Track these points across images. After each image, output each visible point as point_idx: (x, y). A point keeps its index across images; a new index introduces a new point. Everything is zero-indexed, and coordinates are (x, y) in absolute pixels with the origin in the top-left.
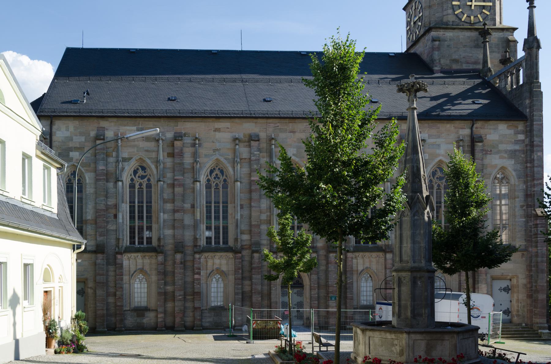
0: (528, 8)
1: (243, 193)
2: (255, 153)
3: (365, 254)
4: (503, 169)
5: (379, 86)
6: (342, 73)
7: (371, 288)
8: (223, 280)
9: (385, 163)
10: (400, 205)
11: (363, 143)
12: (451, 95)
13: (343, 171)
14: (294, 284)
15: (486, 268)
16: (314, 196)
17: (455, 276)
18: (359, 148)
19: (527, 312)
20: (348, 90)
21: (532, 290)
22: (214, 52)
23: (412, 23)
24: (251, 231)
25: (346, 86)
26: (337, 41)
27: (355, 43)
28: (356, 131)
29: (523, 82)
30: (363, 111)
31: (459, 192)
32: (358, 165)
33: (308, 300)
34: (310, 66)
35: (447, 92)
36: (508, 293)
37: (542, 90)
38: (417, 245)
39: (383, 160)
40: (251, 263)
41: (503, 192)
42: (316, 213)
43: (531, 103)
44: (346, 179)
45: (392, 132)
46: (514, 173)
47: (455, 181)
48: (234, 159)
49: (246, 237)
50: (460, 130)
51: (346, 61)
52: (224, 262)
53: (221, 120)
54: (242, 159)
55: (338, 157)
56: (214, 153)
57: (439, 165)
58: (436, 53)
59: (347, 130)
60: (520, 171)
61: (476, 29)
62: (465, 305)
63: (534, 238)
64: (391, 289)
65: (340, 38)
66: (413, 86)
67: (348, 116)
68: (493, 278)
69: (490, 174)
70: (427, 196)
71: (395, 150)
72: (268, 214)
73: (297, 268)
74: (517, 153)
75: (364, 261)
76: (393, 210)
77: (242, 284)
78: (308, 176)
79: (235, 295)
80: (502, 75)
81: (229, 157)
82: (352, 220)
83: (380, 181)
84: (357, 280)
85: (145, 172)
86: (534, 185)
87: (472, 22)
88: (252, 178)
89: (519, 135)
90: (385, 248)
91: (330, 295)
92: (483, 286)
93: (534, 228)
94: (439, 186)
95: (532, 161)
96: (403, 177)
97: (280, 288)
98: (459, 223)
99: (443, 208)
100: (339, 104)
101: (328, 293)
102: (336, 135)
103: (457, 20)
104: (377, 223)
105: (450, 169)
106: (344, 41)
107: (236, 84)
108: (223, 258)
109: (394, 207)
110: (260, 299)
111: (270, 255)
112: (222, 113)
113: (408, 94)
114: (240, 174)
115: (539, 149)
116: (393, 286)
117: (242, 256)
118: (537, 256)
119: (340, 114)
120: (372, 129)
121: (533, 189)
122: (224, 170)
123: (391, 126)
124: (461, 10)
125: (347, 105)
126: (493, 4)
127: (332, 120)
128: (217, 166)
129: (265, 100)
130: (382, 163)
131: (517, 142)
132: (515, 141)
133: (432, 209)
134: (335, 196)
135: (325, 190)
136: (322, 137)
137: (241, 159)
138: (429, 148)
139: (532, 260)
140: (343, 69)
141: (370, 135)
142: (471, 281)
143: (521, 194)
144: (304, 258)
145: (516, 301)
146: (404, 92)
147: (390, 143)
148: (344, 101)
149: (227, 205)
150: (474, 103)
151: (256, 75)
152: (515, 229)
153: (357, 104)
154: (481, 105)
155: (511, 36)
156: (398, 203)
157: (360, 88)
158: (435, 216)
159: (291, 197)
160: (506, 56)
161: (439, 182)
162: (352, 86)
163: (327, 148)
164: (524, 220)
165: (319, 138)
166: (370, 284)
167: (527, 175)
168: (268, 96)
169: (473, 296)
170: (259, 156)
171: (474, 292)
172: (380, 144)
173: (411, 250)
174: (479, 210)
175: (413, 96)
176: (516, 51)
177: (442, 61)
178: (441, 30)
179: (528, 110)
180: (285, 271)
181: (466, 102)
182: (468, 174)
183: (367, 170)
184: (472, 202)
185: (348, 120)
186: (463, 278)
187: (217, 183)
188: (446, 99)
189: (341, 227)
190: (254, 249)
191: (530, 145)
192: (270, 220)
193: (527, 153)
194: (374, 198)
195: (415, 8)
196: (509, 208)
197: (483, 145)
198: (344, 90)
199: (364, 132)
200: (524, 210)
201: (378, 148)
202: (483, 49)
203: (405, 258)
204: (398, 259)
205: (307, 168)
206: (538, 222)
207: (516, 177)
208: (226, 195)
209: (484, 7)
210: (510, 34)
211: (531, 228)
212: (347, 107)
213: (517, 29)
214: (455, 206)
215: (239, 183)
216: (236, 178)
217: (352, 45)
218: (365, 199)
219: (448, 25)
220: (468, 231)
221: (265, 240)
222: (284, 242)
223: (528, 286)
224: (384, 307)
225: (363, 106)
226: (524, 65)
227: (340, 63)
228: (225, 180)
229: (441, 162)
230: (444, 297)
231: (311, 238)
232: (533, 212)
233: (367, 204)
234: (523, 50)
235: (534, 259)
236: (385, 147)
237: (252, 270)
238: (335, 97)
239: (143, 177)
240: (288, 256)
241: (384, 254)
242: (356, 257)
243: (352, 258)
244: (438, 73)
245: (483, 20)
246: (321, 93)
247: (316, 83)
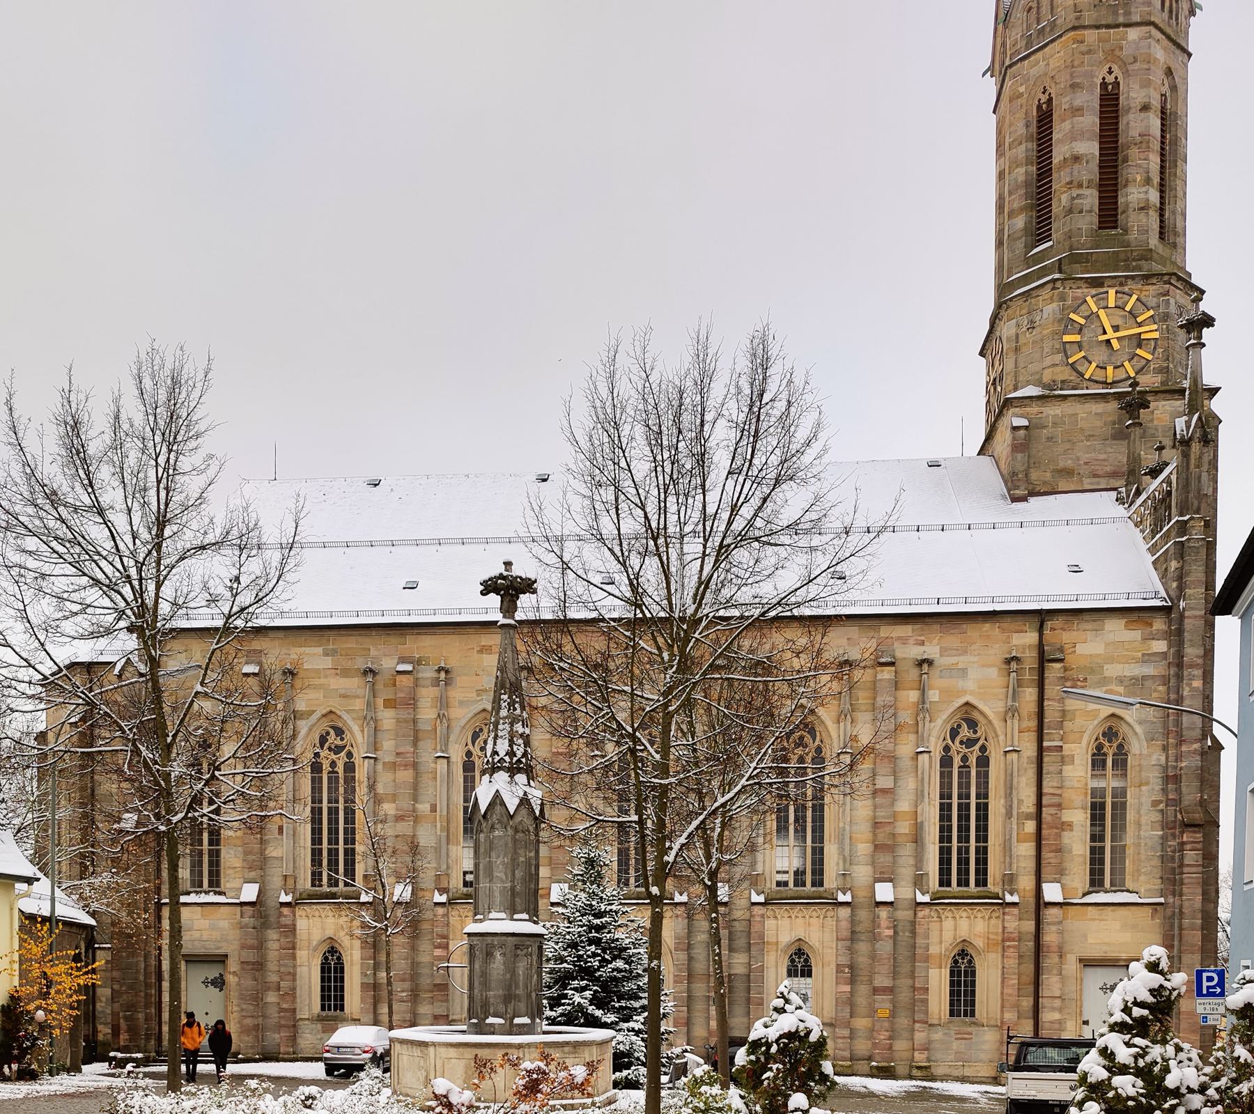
60: (1153, 723)
74: (1148, 683)
85: (342, 739)
87: (1109, 381)
89: (1154, 643)
124: (1082, 354)
131: (1147, 658)
132: (1143, 655)
164: (1161, 833)
197: (1064, 667)
206: (1185, 839)
207: (1143, 737)
239: (337, 750)
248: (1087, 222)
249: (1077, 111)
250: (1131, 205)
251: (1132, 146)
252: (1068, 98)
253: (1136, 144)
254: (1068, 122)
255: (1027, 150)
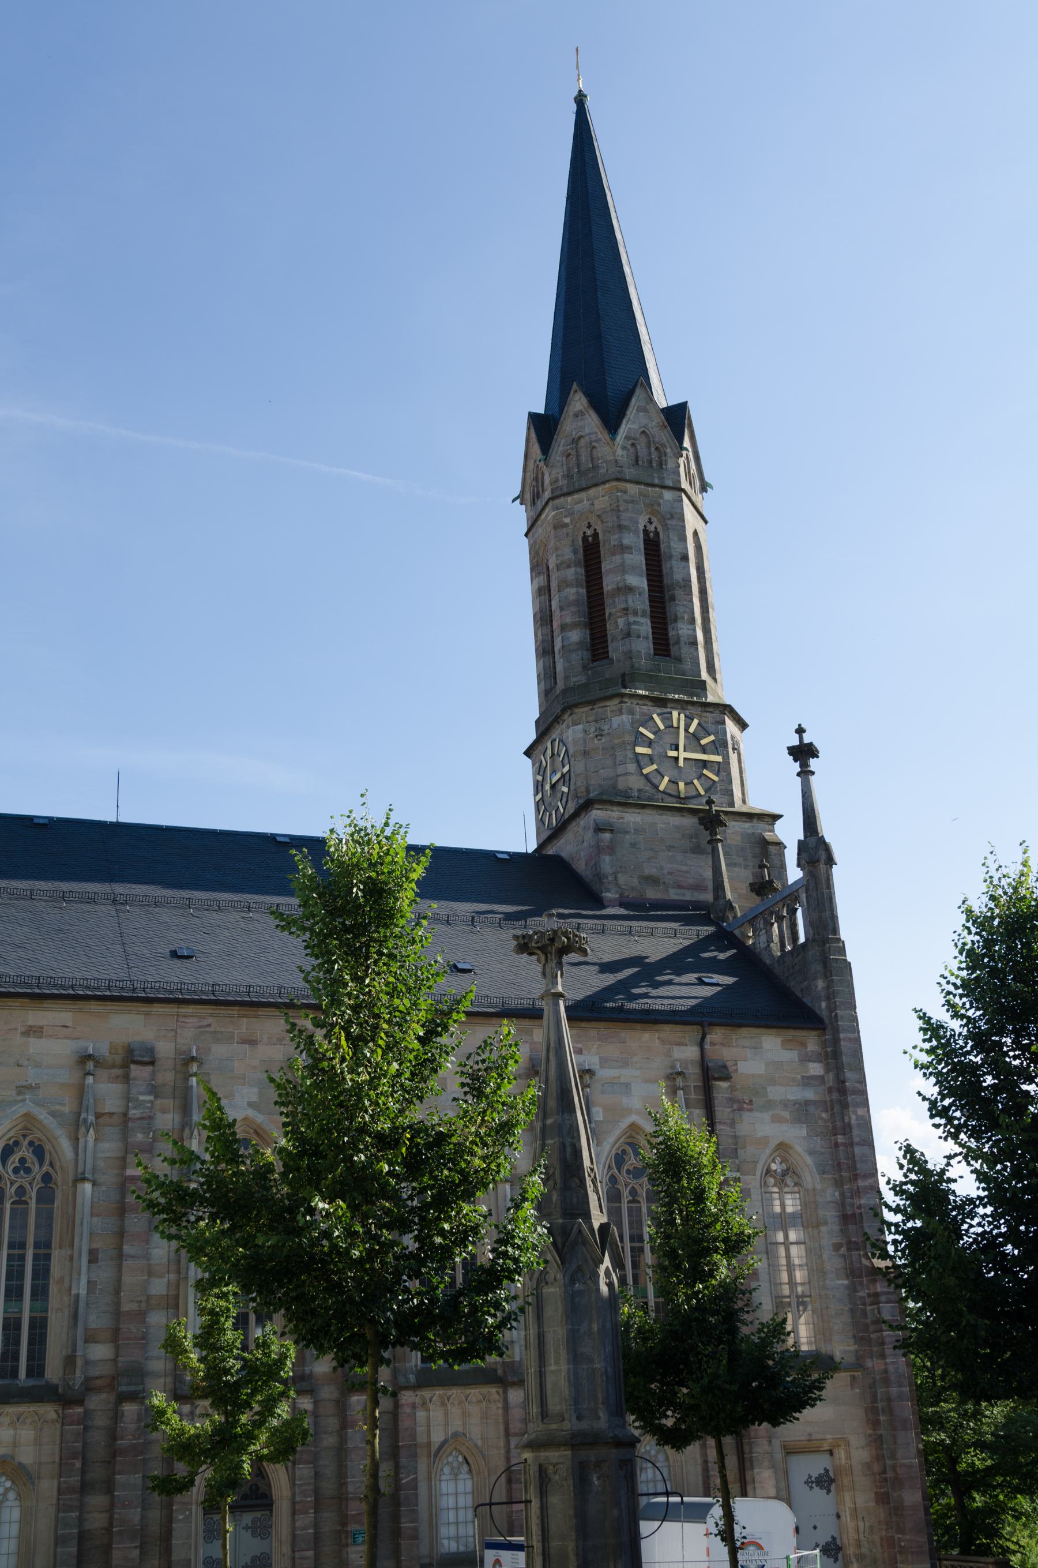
0: (798, 774)
1: (98, 1215)
2: (141, 1098)
3: (449, 1393)
4: (783, 1148)
5: (475, 930)
6: (374, 902)
7: (469, 1498)
8: (19, 1497)
9: (490, 1142)
10: (532, 1256)
11: (431, 1083)
12: (647, 961)
13: (378, 1162)
14: (245, 1497)
15: (765, 1424)
16: (300, 1231)
17: (693, 1450)
18: (421, 1098)
19: (882, 1546)
20: (390, 945)
21: (886, 1480)
22: (41, 821)
23: (547, 787)
24: (116, 1331)
25: (385, 936)
26: (361, 824)
27: (406, 832)
28: (412, 1051)
29: (807, 939)
30: (429, 1001)
31: (681, 1211)
32: (418, 1144)
33: (286, 1549)
34: (291, 881)
35: (638, 954)
36: (829, 1492)
37: (849, 958)
38: (585, 1367)
39: (482, 1131)
40: (113, 1435)
41: (789, 1209)
42: (304, 1282)
43: (828, 987)
44: (388, 1183)
45: (504, 1058)
46: (809, 1160)
47: (670, 1184)
48: (79, 1114)
49: (101, 1351)
50: (676, 1048)
51: (383, 873)
52: (27, 1434)
53: (48, 1004)
54: (104, 1114)
55: (365, 1123)
56: (20, 1098)
57: (630, 1137)
58: (607, 859)
59: (389, 1048)
60: (822, 1154)
61: (693, 812)
62: (723, 1539)
63: (876, 1332)
64: (521, 1502)
65: (369, 817)
66: (552, 940)
67: (390, 1013)
68: (790, 1451)
69: (755, 1162)
70: (602, 1226)
71: (512, 1107)
72: (173, 1276)
73: (252, 1448)
75: (446, 1414)
76: (515, 1270)
77: (82, 1508)
78: (284, 1175)
79: (56, 1545)
80: (760, 919)
81: (62, 1108)
82: (406, 1301)
83: (476, 1188)
84: (430, 1473)
86: (859, 1192)
88: (130, 1172)
90: (504, 1372)
91: (352, 1527)
92: (764, 1476)
93: (872, 1304)
94: (633, 1192)
95: (847, 1129)
96: (536, 1178)
97: (201, 1512)
98: (688, 1299)
99: (648, 1258)
100: (367, 981)
101: (344, 1521)
102: (357, 1061)
103: (648, 788)
104: (474, 1308)
105: (655, 1151)
106: (379, 825)
107: (97, 908)
108: (24, 1422)
109: (516, 1261)
110: (136, 1552)
111: (170, 1411)
112: (49, 986)
113: (543, 957)
114: (94, 1157)
115: (859, 1099)
116: (526, 1492)
117: (87, 1413)
118: (886, 1381)
119: (371, 1006)
120: (453, 1048)
121: (857, 1202)
122: (48, 1147)
123: (501, 1041)
124: (655, 767)
125: (387, 984)
126: (723, 758)
127: (349, 1022)
128: (25, 1136)
129: (174, 955)
130: (481, 1138)
131: (808, 1081)
132: (803, 1077)
133: (618, 1263)
134: (356, 1233)
135: (328, 1214)
136: (320, 1066)
137: (98, 1116)
138: (603, 1092)
139: (876, 1393)
140: (377, 891)
141: (449, 1064)
142: (731, 1462)
143: (831, 1215)
144: (272, 1416)
145: (851, 1515)
146: (531, 954)
147: (499, 1087)
148: (378, 974)
149: (47, 1251)
150: (701, 982)
151: (154, 887)
152: (827, 1308)
153: (411, 983)
154: (719, 988)
155: (769, 831)
156: (528, 1249)
157: (421, 941)
158: (630, 1280)
159: (234, 1234)
160: (763, 877)
161: (633, 1182)
162: (400, 937)
163: (334, 1096)
164: (846, 1282)
165: (312, 1069)
166: (465, 1484)
167: (839, 1164)
168: (184, 945)
169: (741, 1506)
170: (151, 1108)
171: (744, 1494)
172: (475, 1086)
173: (569, 1380)
174: (734, 1261)
175: (554, 965)
176: (783, 866)
177: (622, 879)
178: (615, 808)
179: (824, 1004)
180: (213, 1460)
181: (684, 979)
182: (699, 1166)
183: (443, 1157)
184: (715, 1239)
185: (389, 1022)
186: (712, 1454)
187: (21, 1187)
188: (635, 970)
189: (373, 1322)
190: (123, 1388)
191: (839, 1091)
192: (177, 1297)
193: (832, 1109)
194: (465, 1234)
195: (553, 754)
196: (808, 1251)
198: (380, 946)
199: (433, 1055)
200: (843, 1256)
201: (469, 1098)
202: (710, 856)
203: (554, 1405)
204: (535, 1410)
205: (281, 1151)
206: (879, 1289)
207: (815, 1170)
208: (46, 1220)
209: (705, 764)
210: (767, 827)
211: (864, 1304)
212: (388, 989)
213: (781, 816)
214: (674, 1251)
215: (88, 1186)
216: (80, 1169)
217: (399, 837)
218: (438, 1240)
219: (629, 797)
220: (712, 1320)
221: (158, 1363)
222: (214, 1368)
223: (876, 1468)
224: (505, 1555)
225: (430, 988)
226: (805, 900)
227: (370, 877)
228: (47, 1178)
229: (634, 1127)
230: (667, 1514)
231: (292, 1353)
232: (865, 1262)
233: (445, 1254)
234: (799, 865)
235: (880, 1391)
236: (487, 1097)
237: (114, 1456)
238: (356, 961)
240: (226, 1413)
241: (501, 1391)
242: (424, 1404)
243: (414, 1406)
244: (613, 906)
245: (706, 791)
246: (319, 949)
247: (308, 924)
248: (644, 646)
249: (623, 549)
250: (682, 639)
251: (677, 588)
252: (616, 536)
253: (680, 587)
254: (618, 557)
255: (576, 573)
